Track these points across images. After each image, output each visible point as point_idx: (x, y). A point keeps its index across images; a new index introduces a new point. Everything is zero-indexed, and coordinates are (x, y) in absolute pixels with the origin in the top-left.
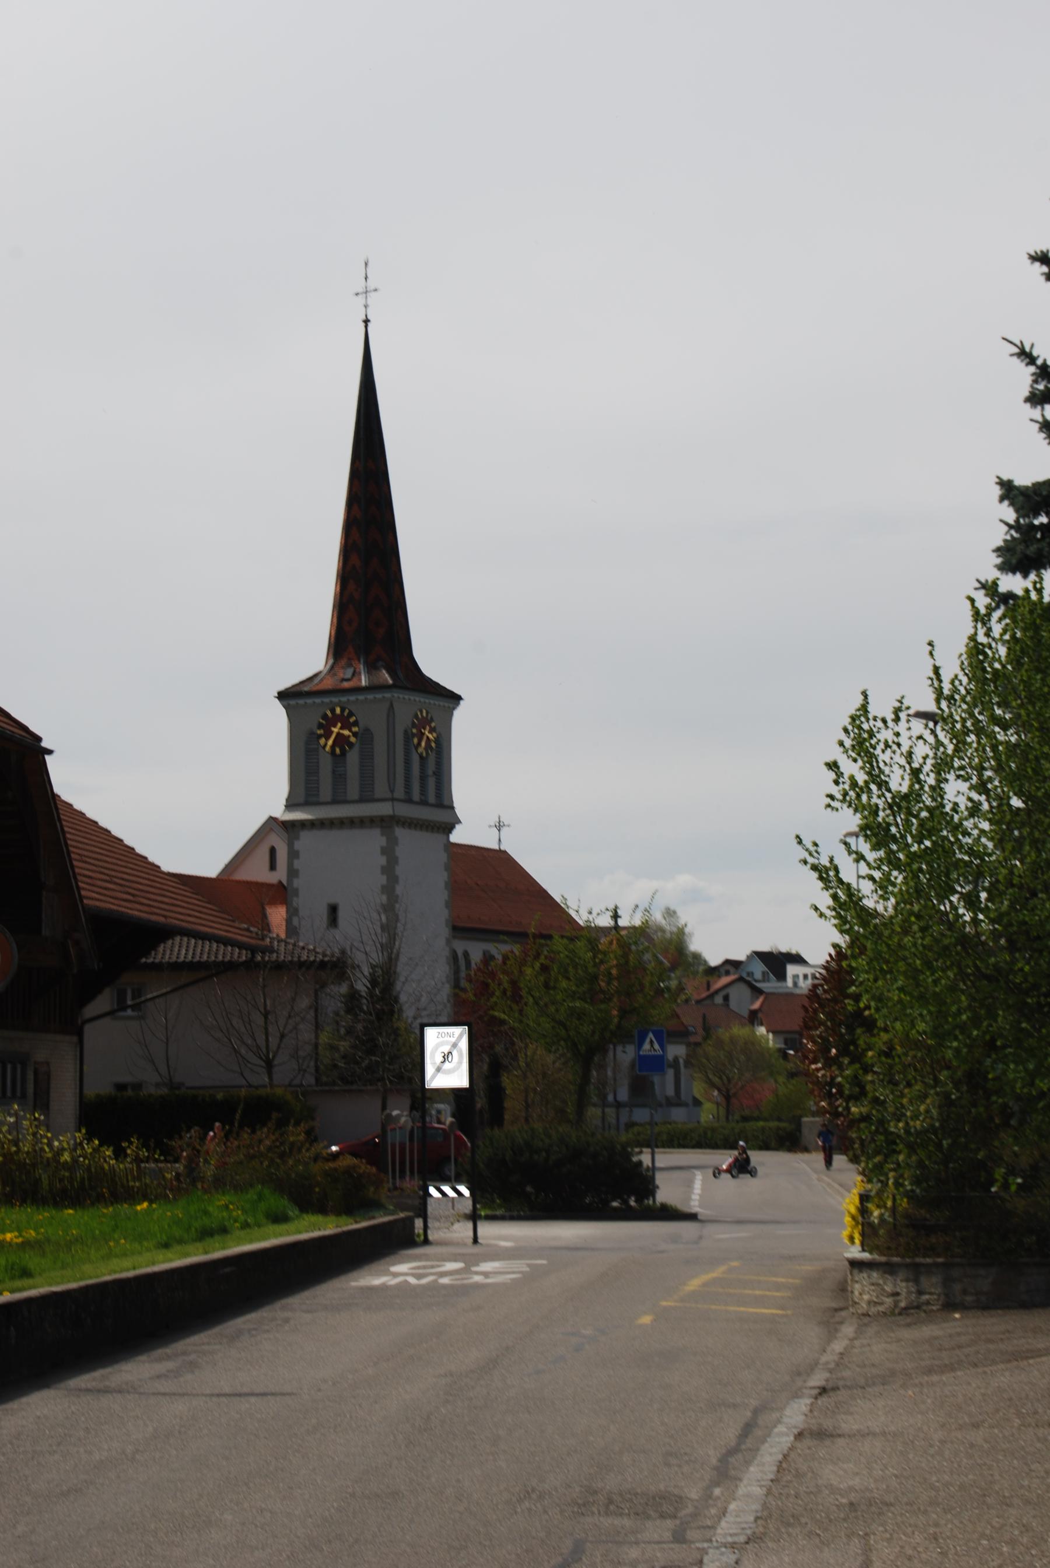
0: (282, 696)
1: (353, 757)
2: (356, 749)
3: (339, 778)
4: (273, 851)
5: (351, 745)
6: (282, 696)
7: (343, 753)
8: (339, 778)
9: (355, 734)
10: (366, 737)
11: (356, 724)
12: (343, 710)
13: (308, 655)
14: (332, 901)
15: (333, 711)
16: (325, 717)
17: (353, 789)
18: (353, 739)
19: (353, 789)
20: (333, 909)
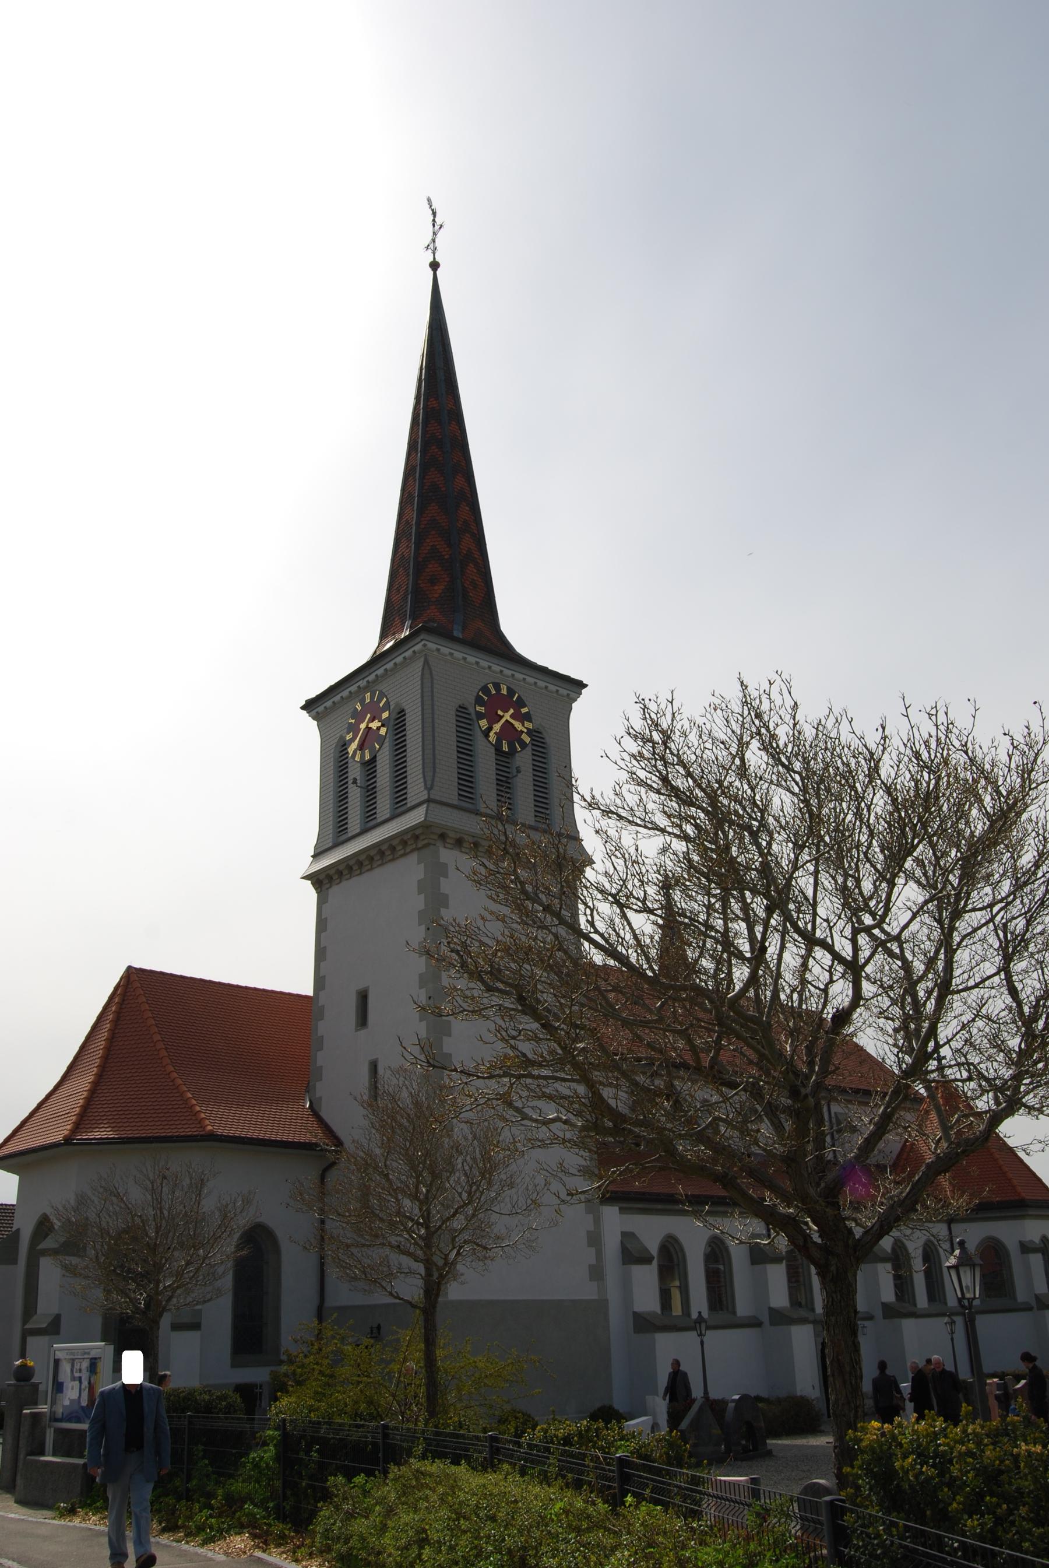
5: (523, 745)
9: (529, 732)
11: (527, 717)
12: (511, 692)
13: (347, 625)
14: (361, 986)
15: (497, 686)
16: (485, 689)
18: (527, 739)
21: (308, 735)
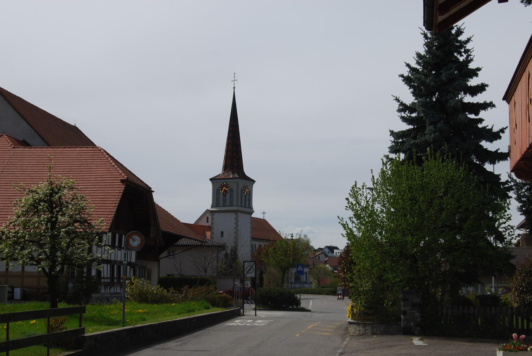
0: (211, 179)
1: (228, 195)
2: (229, 193)
3: (225, 200)
4: (208, 218)
6: (211, 179)
7: (226, 194)
8: (225, 200)
10: (231, 190)
11: (229, 187)
13: (217, 169)
17: (228, 203)
19: (228, 203)
20: (222, 233)
21: (209, 186)
